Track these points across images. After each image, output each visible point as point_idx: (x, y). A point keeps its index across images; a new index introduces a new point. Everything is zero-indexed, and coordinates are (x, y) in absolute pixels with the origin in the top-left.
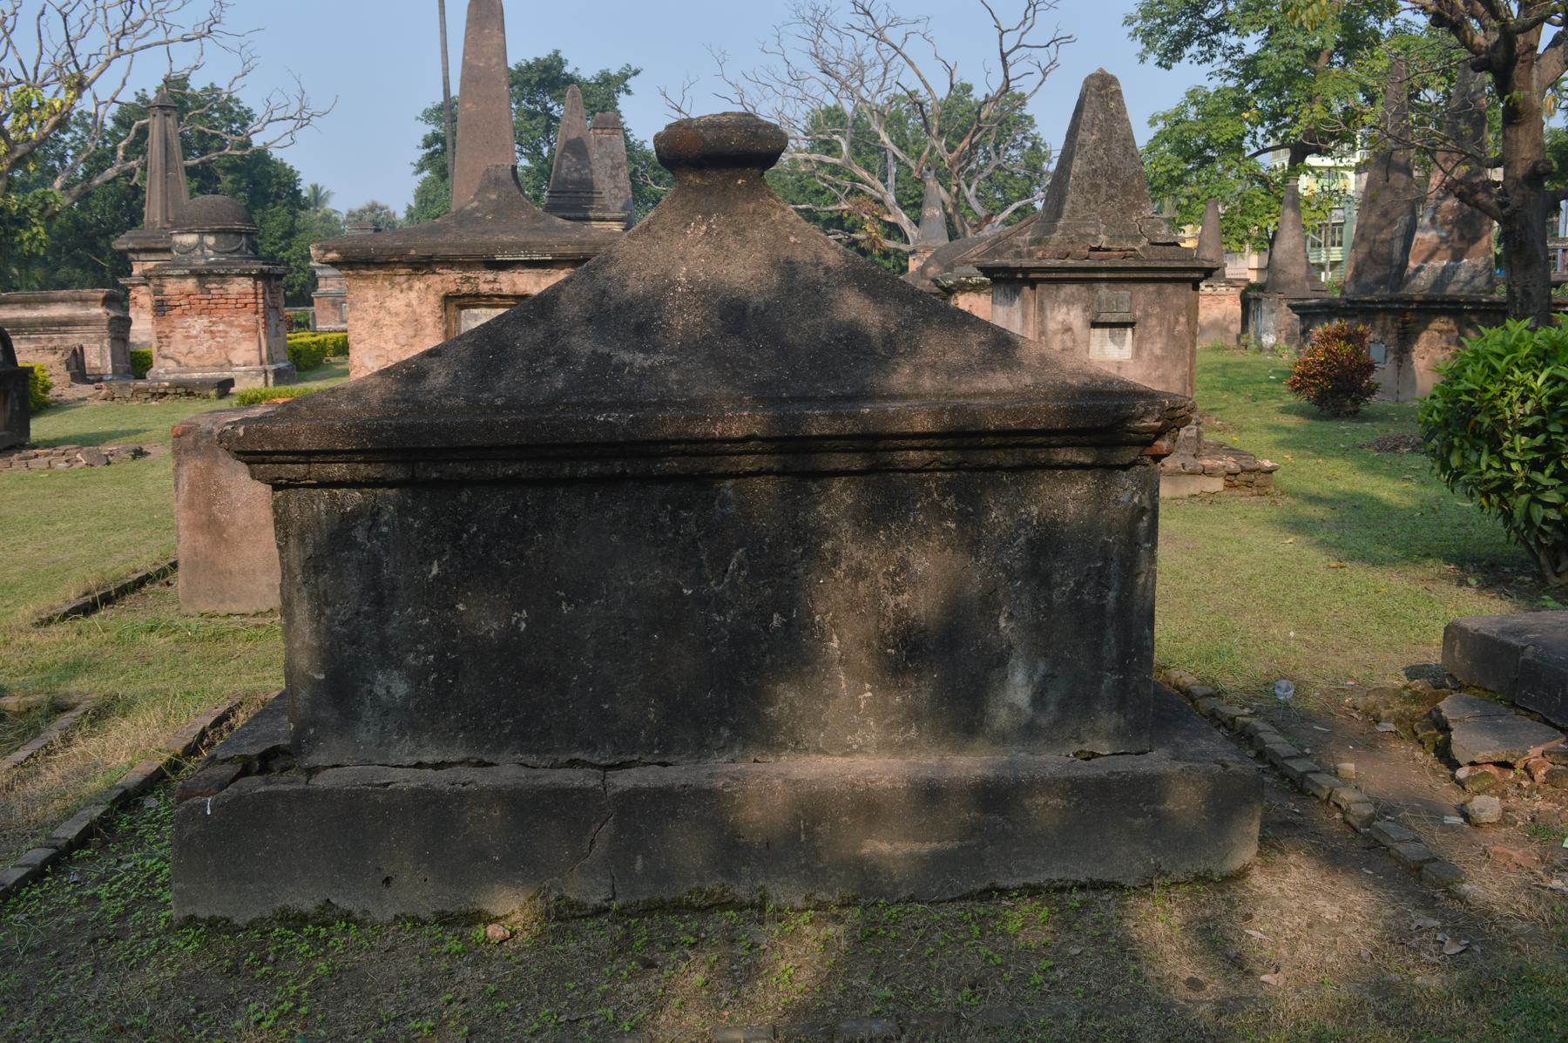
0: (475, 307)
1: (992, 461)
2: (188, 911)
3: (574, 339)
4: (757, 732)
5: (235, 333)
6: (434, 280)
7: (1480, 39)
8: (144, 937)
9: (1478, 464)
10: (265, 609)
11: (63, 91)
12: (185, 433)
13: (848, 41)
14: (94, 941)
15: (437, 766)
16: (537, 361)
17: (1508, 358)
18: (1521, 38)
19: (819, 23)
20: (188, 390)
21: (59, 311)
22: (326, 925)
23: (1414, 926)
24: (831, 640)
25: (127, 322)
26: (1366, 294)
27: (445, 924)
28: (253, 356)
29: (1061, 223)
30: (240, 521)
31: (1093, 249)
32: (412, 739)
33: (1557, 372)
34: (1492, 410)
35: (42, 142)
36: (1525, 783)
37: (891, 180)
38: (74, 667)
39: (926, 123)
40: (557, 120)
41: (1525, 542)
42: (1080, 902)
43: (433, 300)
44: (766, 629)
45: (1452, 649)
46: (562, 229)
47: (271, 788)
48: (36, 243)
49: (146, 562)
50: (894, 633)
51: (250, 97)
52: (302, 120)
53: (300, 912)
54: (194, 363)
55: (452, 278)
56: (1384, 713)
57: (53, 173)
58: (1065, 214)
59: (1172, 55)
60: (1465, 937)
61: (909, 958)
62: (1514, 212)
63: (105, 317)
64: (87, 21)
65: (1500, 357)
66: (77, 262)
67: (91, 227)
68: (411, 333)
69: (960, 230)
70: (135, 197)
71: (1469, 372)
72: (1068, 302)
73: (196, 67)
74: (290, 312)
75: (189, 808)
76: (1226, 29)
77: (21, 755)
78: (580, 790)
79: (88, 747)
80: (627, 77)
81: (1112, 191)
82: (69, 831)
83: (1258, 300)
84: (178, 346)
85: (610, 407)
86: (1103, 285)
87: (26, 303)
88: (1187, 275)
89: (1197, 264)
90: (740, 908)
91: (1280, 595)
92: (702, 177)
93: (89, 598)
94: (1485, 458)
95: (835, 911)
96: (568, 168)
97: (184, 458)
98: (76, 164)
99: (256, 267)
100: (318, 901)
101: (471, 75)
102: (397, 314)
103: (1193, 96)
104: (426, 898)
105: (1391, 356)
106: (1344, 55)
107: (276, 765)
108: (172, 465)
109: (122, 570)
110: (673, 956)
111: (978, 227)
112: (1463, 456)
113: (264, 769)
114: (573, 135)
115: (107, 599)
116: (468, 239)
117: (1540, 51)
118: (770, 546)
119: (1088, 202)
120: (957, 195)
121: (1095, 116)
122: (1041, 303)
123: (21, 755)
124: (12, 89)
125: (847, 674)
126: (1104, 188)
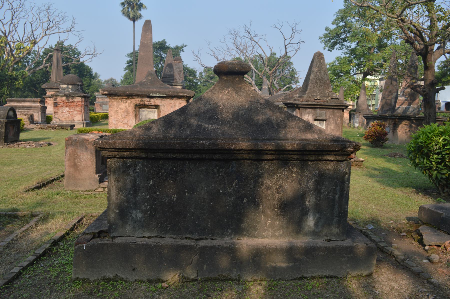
0: (144, 108)
1: (306, 158)
2: (77, 276)
3: (192, 120)
4: (239, 230)
5: (76, 112)
6: (133, 100)
7: (418, 47)
8: (64, 283)
9: (423, 162)
10: (88, 190)
11: (30, 44)
12: (69, 140)
13: (243, 40)
14: (50, 284)
15: (149, 237)
16: (182, 126)
17: (432, 134)
18: (429, 47)
19: (236, 35)
20: (62, 127)
21: (27, 104)
22: (116, 281)
23: (420, 291)
24: (260, 206)
25: (46, 108)
26: (384, 114)
27: (149, 282)
28: (80, 119)
29: (307, 92)
30: (83, 165)
31: (315, 99)
32: (142, 229)
33: (446, 138)
34: (427, 146)
35: (23, 58)
36: (444, 251)
37: (254, 78)
38: (41, 204)
39: (264, 63)
40: (163, 58)
41: (435, 184)
42: (328, 281)
43: (132, 106)
44: (242, 202)
45: (421, 213)
46: (169, 88)
47: (103, 242)
48: (20, 85)
49: (54, 175)
50: (277, 205)
51: (80, 48)
52: (94, 55)
53: (109, 278)
54: (64, 120)
56: (403, 230)
57: (25, 66)
58: (308, 90)
59: (332, 47)
60: (434, 294)
61: (281, 296)
62: (427, 93)
63: (40, 106)
64: (37, 26)
65: (430, 133)
66: (30, 91)
67: (35, 81)
69: (272, 92)
70: (47, 74)
71: (421, 137)
72: (309, 113)
73: (66, 40)
74: (90, 106)
75: (79, 247)
76: (346, 41)
77: (24, 229)
78: (190, 246)
79: (43, 227)
80: (183, 47)
81: (321, 84)
82: (40, 251)
83: (354, 114)
84: (60, 115)
85: (203, 139)
86: (318, 109)
87: (18, 101)
88: (341, 107)
89: (344, 105)
90: (232, 280)
92: (227, 77)
93: (39, 184)
94: (425, 160)
95: (259, 282)
96: (167, 71)
97: (68, 147)
98: (32, 64)
99: (82, 94)
100: (114, 275)
101: (142, 45)
102: (122, 109)
103: (337, 59)
104: (145, 275)
105: (391, 131)
106: (378, 49)
107: (102, 235)
108: (64, 149)
109: (48, 177)
110: (215, 293)
111: (277, 91)
112: (419, 160)
113: (99, 237)
114: (169, 62)
115: (44, 185)
116: (143, 90)
117: (434, 51)
118: (245, 180)
119: (314, 87)
120: (271, 83)
121: (317, 64)
122: (301, 113)
123: (24, 229)
124: (16, 43)
125: (264, 215)
126: (319, 83)
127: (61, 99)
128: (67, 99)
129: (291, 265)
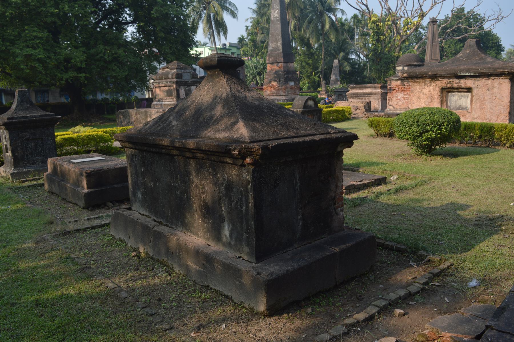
0: (454, 92)
6: (438, 82)
21: (368, 90)
43: (438, 89)
51: (480, 11)
52: (498, 20)
54: (398, 107)
55: (444, 82)
63: (380, 92)
68: (430, 101)
91: (496, 251)
102: (426, 94)
127: (395, 83)
128: (402, 83)
129: (202, 270)
